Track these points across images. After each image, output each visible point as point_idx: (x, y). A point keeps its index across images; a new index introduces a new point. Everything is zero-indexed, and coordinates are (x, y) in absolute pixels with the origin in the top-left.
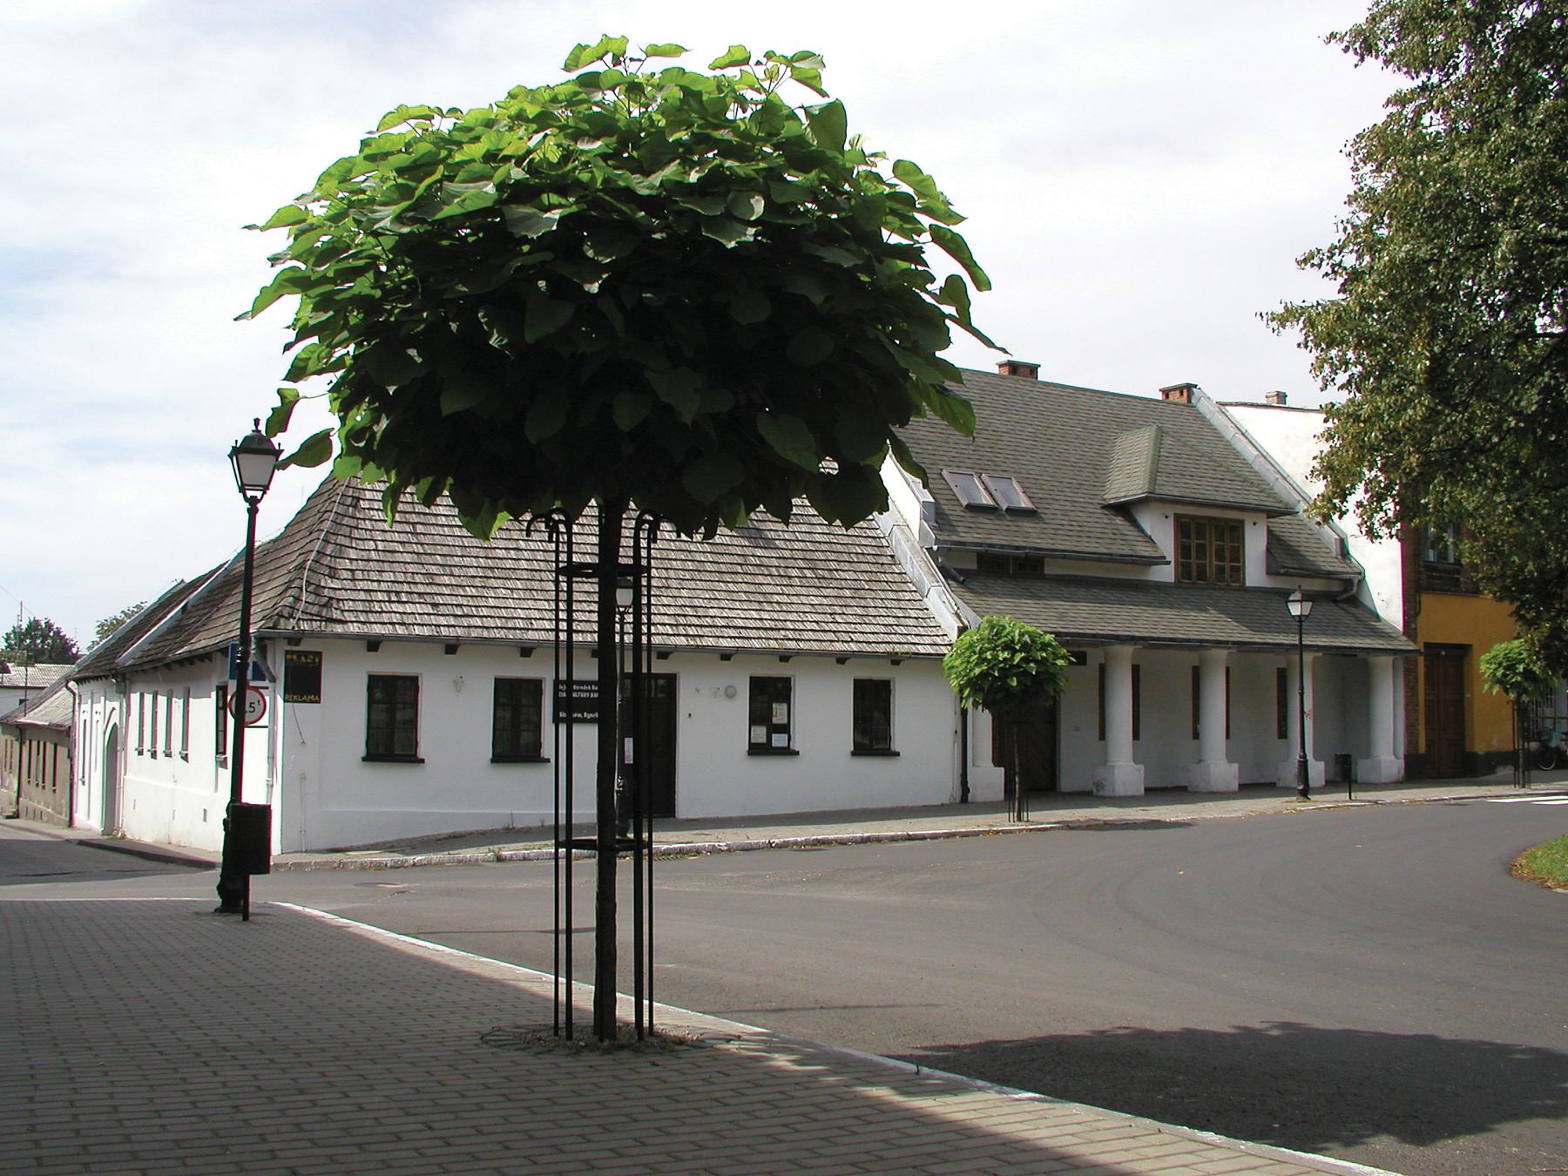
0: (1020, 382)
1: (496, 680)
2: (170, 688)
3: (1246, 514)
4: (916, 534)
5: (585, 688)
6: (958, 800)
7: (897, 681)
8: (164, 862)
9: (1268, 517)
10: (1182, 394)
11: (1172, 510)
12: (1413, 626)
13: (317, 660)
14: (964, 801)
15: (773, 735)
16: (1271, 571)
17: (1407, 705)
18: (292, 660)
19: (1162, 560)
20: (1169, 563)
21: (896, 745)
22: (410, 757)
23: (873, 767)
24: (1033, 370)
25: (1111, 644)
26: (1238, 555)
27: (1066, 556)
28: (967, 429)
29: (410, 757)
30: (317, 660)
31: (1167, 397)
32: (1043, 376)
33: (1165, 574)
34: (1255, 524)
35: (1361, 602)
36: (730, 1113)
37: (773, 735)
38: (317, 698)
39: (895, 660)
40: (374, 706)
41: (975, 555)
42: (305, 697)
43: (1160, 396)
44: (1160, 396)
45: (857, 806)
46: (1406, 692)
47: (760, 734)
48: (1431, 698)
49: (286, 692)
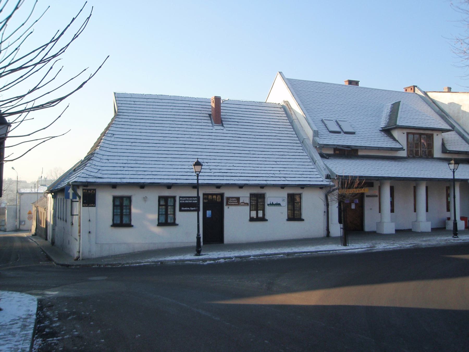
3: (433, 131)
4: (311, 141)
5: (191, 199)
6: (325, 236)
10: (411, 89)
11: (405, 131)
13: (94, 192)
14: (327, 238)
18: (85, 192)
19: (402, 149)
20: (404, 150)
22: (300, 219)
23: (295, 224)
24: (357, 83)
25: (382, 180)
27: (366, 148)
28: (399, 102)
29: (300, 219)
30: (94, 192)
31: (406, 90)
32: (360, 85)
34: (437, 135)
38: (94, 205)
39: (303, 187)
40: (160, 207)
42: (90, 205)
44: (404, 91)
45: (295, 237)
47: (254, 214)
49: (83, 203)
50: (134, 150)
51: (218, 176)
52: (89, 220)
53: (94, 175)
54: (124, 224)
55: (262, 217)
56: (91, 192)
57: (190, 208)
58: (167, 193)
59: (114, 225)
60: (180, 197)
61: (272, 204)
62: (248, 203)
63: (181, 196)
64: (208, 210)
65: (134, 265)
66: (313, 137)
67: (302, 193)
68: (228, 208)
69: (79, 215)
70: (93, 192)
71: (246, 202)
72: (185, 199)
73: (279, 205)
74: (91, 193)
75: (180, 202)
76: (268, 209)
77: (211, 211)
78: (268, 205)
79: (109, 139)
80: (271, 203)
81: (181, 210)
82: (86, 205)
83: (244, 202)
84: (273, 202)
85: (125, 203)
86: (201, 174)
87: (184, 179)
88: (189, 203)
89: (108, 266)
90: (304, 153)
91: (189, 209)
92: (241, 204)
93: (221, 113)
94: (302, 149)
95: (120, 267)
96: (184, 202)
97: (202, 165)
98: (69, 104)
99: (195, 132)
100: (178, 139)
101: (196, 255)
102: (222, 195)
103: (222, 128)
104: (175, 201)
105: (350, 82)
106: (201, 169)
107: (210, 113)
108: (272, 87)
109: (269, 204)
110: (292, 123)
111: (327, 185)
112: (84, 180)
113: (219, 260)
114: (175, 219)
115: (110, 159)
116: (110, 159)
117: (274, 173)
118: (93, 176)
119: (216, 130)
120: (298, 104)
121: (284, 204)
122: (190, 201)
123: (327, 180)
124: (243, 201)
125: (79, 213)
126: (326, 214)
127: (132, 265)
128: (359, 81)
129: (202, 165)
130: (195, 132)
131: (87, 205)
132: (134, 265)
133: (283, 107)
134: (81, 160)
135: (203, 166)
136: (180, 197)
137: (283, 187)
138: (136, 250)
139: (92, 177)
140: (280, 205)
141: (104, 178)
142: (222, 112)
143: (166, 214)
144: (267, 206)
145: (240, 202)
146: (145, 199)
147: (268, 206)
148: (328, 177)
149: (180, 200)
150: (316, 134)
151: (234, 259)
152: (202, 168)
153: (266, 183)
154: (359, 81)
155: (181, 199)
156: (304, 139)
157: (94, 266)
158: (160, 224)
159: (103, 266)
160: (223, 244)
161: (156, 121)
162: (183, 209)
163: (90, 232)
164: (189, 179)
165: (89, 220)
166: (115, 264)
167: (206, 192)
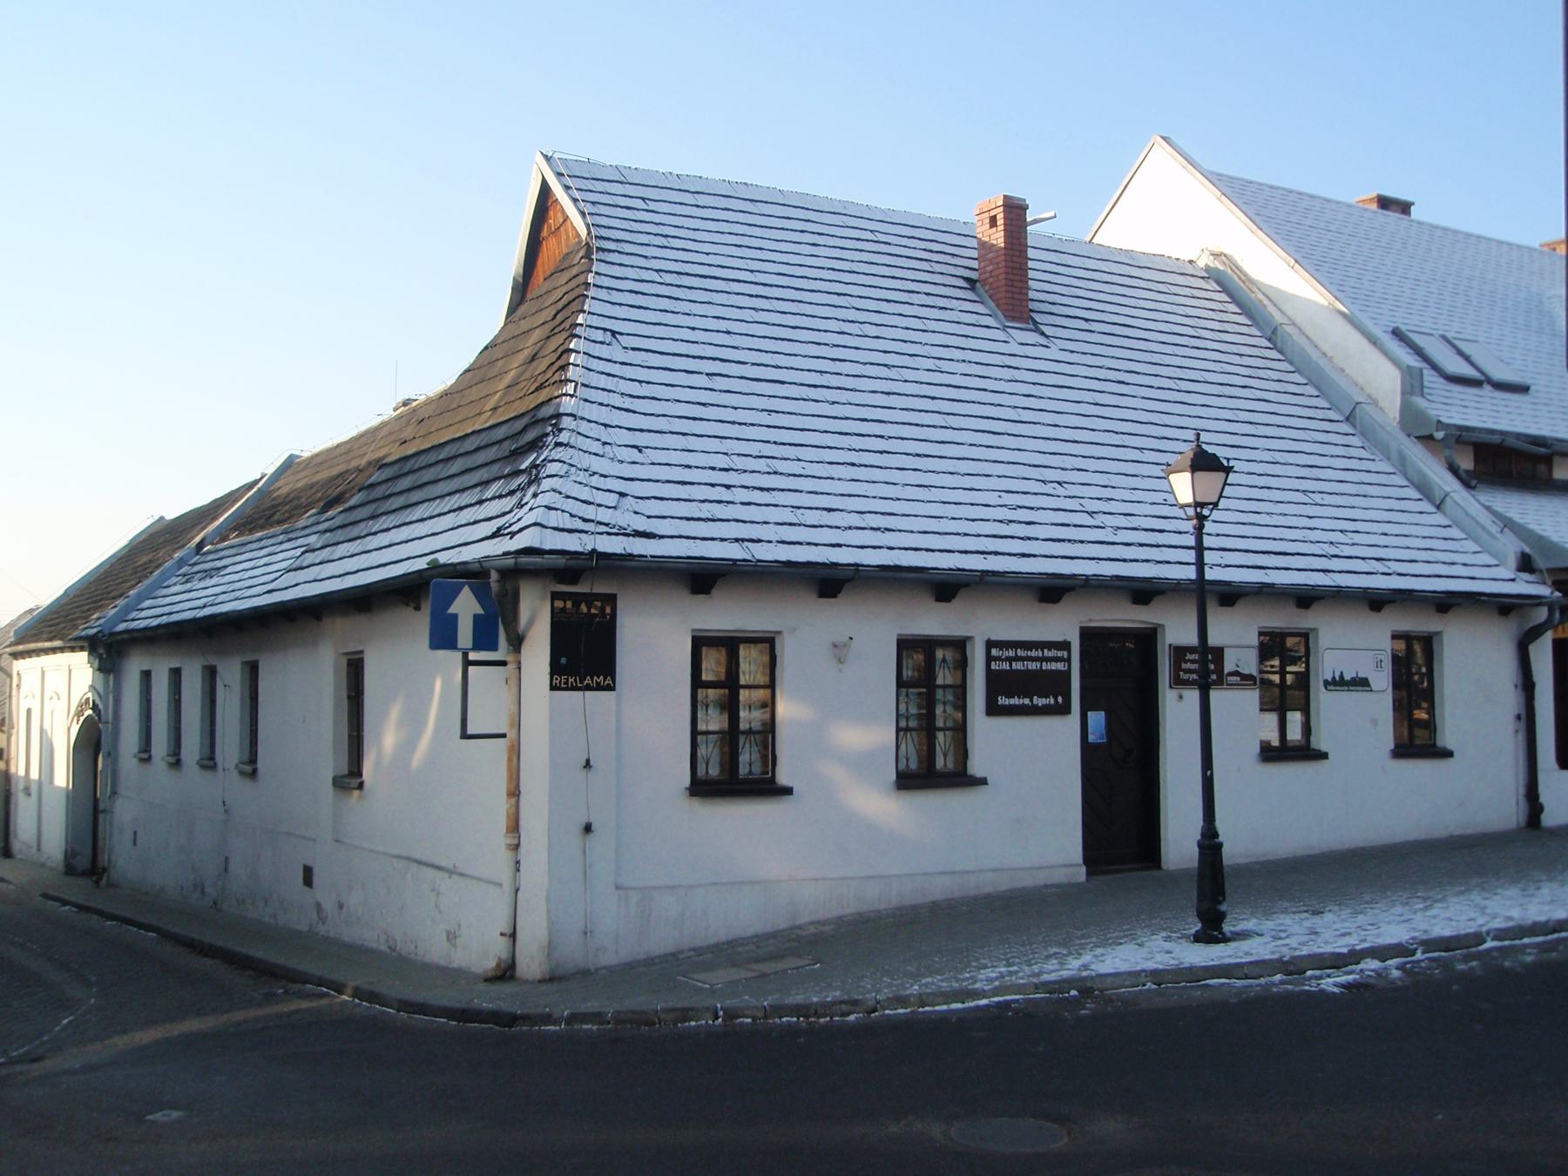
0: (1392, 217)
2: (212, 660)
5: (1033, 653)
6: (1523, 819)
7: (1446, 638)
13: (608, 610)
15: (1089, 713)
24: (1404, 208)
30: (608, 610)
37: (1089, 713)
42: (588, 681)
49: (555, 669)
50: (736, 408)
51: (1141, 545)
52: (588, 765)
53: (613, 522)
54: (746, 781)
55: (1299, 741)
56: (593, 611)
57: (1031, 701)
58: (933, 621)
59: (701, 788)
60: (990, 644)
61: (1338, 683)
63: (994, 638)
64: (1090, 710)
65: (937, 1008)
66: (1403, 393)
67: (1439, 633)
68: (1181, 697)
69: (512, 735)
70: (602, 609)
71: (1246, 671)
72: (1011, 653)
73: (1361, 683)
74: (595, 615)
75: (993, 668)
76: (1325, 702)
77: (1103, 713)
78: (1326, 683)
79: (597, 350)
80: (1337, 679)
81: (993, 710)
82: (566, 683)
83: (1240, 670)
84: (1342, 673)
85: (750, 665)
86: (1216, 515)
87: (1015, 555)
88: (1028, 672)
89: (784, 1019)
90: (1376, 463)
91: (1027, 701)
92: (1229, 678)
93: (1030, 271)
94: (1361, 445)
95: (825, 1027)
96: (1006, 666)
97: (1228, 470)
99: (948, 346)
100: (893, 373)
101: (1202, 938)
102: (1147, 638)
103: (1032, 337)
104: (962, 664)
105: (1385, 203)
106: (1225, 484)
107: (974, 275)
108: (1113, 207)
109: (1330, 680)
110: (1273, 336)
111: (1544, 597)
112: (571, 543)
113: (1359, 963)
114: (963, 753)
115: (647, 447)
116: (647, 447)
117: (1332, 540)
118: (607, 525)
119: (1022, 344)
120: (1292, 262)
121: (1382, 680)
122: (1030, 663)
123: (1526, 576)
124: (1237, 666)
125: (511, 725)
126: (1522, 725)
127: (927, 1008)
128: (1413, 204)
129: (1228, 470)
130: (948, 346)
131: (571, 680)
132: (937, 1008)
133: (1211, 275)
134: (156, 518)
135: (1231, 474)
136: (990, 644)
137: (1377, 601)
138: (804, 918)
139: (603, 529)
140: (1369, 685)
141: (662, 537)
142: (1030, 269)
143: (927, 727)
144: (1325, 690)
145: (1226, 672)
146: (840, 651)
147: (1326, 688)
148: (1526, 564)
149: (989, 659)
150: (1412, 385)
151: (1419, 956)
152: (1228, 482)
153: (1328, 584)
154: (1413, 204)
155: (994, 652)
156: (1358, 403)
157: (693, 1023)
158: (907, 781)
159: (754, 1018)
160: (1155, 873)
161: (768, 288)
162: (1002, 701)
163: (588, 828)
164: (1035, 556)
165: (588, 765)
166: (824, 1005)
167: (1090, 620)
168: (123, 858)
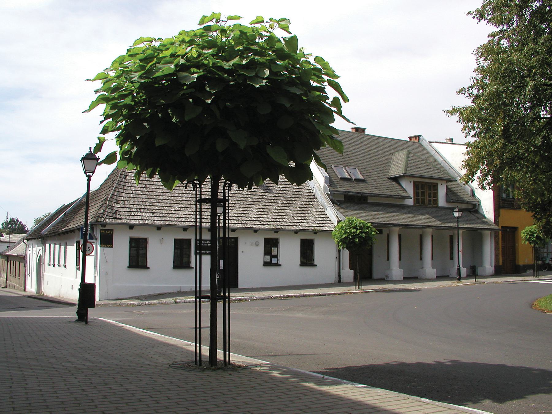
0: (359, 134)
1: (175, 239)
2: (60, 242)
3: (438, 181)
4: (323, 188)
5: (206, 242)
6: (337, 282)
7: (316, 240)
8: (58, 303)
9: (447, 182)
10: (416, 139)
11: (412, 180)
12: (498, 220)
13: (112, 232)
14: (339, 282)
15: (272, 259)
16: (447, 201)
17: (495, 248)
18: (103, 232)
19: (409, 197)
20: (411, 198)
21: (316, 262)
23: (307, 270)
24: (364, 130)
25: (391, 227)
26: (436, 195)
27: (375, 196)
30: (112, 232)
31: (411, 140)
32: (367, 132)
33: (410, 202)
34: (442, 184)
35: (479, 212)
36: (257, 392)
37: (272, 259)
38: (112, 246)
39: (315, 232)
41: (343, 195)
42: (107, 246)
43: (408, 140)
44: (408, 140)
46: (495, 244)
47: (268, 258)
48: (504, 246)
49: (101, 243)
62: (462, 231)
98: (72, 289)
168: (474, 276)
